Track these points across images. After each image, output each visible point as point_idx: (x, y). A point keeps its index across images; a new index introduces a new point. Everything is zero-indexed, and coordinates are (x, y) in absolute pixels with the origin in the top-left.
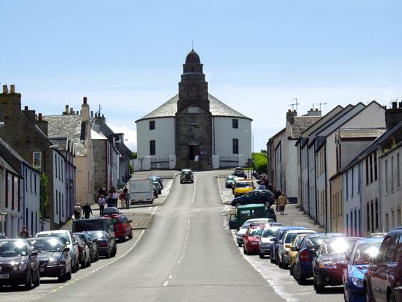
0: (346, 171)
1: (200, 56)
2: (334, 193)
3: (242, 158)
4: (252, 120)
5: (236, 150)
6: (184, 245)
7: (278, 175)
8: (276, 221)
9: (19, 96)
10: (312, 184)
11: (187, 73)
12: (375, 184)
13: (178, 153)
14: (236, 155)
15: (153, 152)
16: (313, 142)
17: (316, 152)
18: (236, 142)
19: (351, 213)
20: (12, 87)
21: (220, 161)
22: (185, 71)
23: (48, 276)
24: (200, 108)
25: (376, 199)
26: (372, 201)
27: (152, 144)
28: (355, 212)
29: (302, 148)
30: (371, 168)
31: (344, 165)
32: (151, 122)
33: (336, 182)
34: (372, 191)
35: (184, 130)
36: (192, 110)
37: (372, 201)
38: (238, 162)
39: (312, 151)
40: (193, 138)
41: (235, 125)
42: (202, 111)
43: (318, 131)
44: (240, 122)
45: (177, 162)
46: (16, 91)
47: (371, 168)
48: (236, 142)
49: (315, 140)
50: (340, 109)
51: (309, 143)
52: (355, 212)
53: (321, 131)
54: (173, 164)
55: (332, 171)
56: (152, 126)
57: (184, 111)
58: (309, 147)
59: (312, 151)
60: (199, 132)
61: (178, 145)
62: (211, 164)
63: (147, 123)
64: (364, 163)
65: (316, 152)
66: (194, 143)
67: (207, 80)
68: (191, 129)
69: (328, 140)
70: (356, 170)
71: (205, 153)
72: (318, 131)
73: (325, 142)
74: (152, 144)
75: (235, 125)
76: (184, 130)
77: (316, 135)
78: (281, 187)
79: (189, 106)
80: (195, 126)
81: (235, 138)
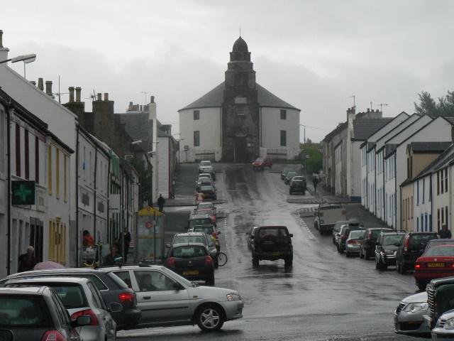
0: (417, 179)
1: (246, 41)
2: (404, 198)
3: (292, 152)
4: (300, 111)
5: (283, 142)
9: (112, 103)
10: (379, 186)
11: (235, 62)
12: (446, 195)
13: (224, 145)
14: (284, 147)
15: (196, 143)
16: (382, 149)
18: (283, 134)
19: (422, 217)
20: (106, 95)
21: (268, 154)
22: (232, 59)
25: (447, 207)
26: (443, 209)
27: (196, 134)
28: (426, 216)
30: (442, 182)
31: (414, 176)
32: (195, 112)
34: (441, 201)
36: (240, 100)
37: (443, 209)
38: (286, 154)
39: (381, 155)
41: (283, 116)
44: (289, 112)
46: (110, 99)
47: (442, 182)
48: (283, 134)
49: (383, 147)
50: (403, 118)
51: (377, 149)
52: (426, 216)
53: (389, 140)
55: (403, 176)
56: (196, 116)
58: (377, 153)
59: (381, 155)
63: (191, 113)
64: (435, 177)
65: (385, 158)
67: (254, 69)
69: (398, 150)
70: (421, 182)
71: (253, 145)
73: (395, 151)
75: (283, 116)
77: (386, 143)
79: (235, 97)
81: (283, 129)
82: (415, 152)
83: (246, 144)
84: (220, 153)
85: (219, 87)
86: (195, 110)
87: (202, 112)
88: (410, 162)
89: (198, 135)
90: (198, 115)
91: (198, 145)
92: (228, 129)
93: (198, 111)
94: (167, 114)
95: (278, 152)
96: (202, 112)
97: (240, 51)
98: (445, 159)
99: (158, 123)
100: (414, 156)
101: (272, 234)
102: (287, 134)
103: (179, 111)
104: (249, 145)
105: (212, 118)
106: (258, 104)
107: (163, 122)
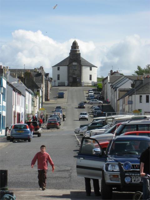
2: (118, 104)
5: (91, 79)
6: (135, 175)
7: (105, 93)
8: (110, 102)
13: (68, 80)
15: (58, 79)
17: (115, 91)
23: (129, 131)
24: (78, 63)
27: (58, 76)
29: (112, 88)
33: (118, 101)
35: (71, 71)
36: (74, 64)
40: (74, 74)
42: (78, 64)
43: (116, 85)
44: (93, 68)
45: (68, 83)
48: (91, 76)
54: (66, 84)
55: (118, 98)
56: (59, 69)
57: (71, 64)
60: (77, 72)
61: (69, 77)
62: (81, 84)
63: (57, 67)
65: (115, 91)
66: (75, 76)
68: (74, 71)
72: (116, 85)
74: (58, 76)
75: (91, 69)
76: (71, 71)
78: (59, 171)
80: (76, 70)
82: (120, 91)
83: (77, 80)
84: (67, 83)
85: (67, 58)
86: (58, 66)
87: (61, 67)
88: (119, 93)
89: (59, 76)
90: (59, 69)
91: (59, 80)
92: (70, 74)
93: (59, 67)
94: (48, 69)
95: (89, 83)
96: (61, 67)
97: (75, 46)
98: (16, 118)
99: (45, 72)
100: (120, 92)
101: (126, 123)
102: (89, 79)
103: (52, 67)
104: (78, 80)
105: (64, 69)
106: (81, 65)
107: (46, 72)
